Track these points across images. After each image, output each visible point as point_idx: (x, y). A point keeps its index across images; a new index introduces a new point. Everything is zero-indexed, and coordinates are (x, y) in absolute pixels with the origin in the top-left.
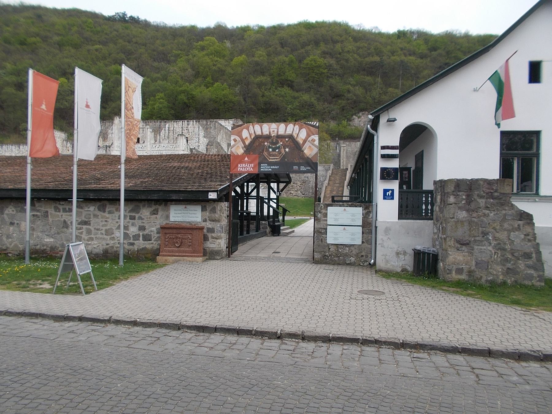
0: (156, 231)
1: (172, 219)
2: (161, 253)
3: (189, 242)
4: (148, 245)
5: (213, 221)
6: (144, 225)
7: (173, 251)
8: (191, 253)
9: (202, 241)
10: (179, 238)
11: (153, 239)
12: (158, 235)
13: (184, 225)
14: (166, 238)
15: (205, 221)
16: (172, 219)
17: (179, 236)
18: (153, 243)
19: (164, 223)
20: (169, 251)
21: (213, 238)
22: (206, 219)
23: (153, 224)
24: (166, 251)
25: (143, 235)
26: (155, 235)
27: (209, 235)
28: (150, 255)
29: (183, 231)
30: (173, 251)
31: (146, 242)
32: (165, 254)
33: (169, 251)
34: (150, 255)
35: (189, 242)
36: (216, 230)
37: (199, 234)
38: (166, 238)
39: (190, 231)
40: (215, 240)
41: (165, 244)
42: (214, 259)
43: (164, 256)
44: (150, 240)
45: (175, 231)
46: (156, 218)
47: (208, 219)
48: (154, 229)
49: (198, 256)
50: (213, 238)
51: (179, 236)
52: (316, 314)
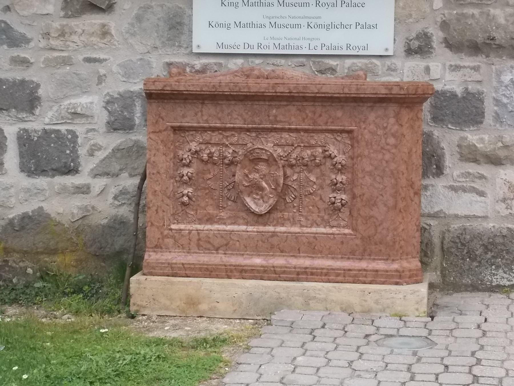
0: (102, 117)
1: (205, 38)
2: (151, 257)
3: (335, 186)
4: (58, 200)
5: (475, 48)
6: (31, 75)
7: (226, 244)
8: (351, 254)
9: (416, 177)
10: (271, 161)
11: (88, 165)
12: (117, 140)
13: (297, 75)
14: (180, 163)
15: (419, 47)
16: (205, 38)
17: (268, 145)
18: (83, 190)
19: (159, 65)
20: (204, 244)
21: (471, 155)
22: (425, 38)
23: (85, 70)
24: (181, 242)
25: (24, 139)
26: (97, 142)
27: (449, 139)
28: (69, 259)
29: (291, 116)
30: (226, 244)
31: (42, 182)
32: (176, 257)
33: (204, 244)
34: (69, 259)
35: (335, 186)
36: (490, 108)
37: (399, 137)
38: (180, 163)
39: (342, 119)
40: (484, 170)
41: (176, 197)
42: (474, 288)
43: (175, 271)
44: (70, 170)
45: (237, 116)
46: (105, 33)
47: (437, 36)
48: (91, 101)
49: (398, 278)
50: (471, 155)
51: (268, 145)
52: (355, 343)
